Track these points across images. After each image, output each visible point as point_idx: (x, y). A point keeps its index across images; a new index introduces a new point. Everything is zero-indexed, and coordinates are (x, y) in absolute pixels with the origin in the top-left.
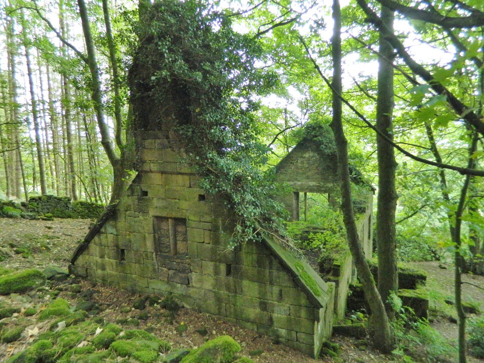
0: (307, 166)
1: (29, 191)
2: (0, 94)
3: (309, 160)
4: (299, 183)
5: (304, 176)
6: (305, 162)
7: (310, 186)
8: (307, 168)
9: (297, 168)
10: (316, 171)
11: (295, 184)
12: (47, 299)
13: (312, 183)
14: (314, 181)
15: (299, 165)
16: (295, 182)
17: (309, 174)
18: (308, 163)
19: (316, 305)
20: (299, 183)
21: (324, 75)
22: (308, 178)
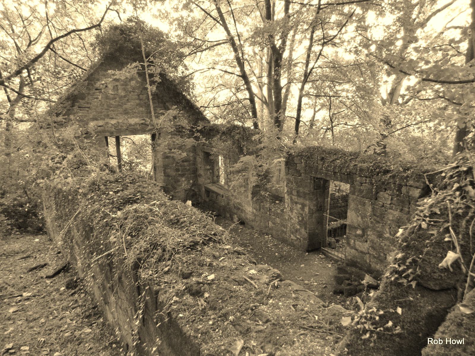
0: (123, 94)
1: (420, 190)
2: (1, 158)
3: (126, 85)
4: (113, 122)
5: (120, 110)
6: (119, 87)
7: (130, 125)
8: (125, 96)
9: (107, 97)
10: (138, 101)
11: (107, 123)
12: (160, 342)
13: (133, 121)
14: (137, 117)
15: (111, 92)
16: (107, 120)
17: (128, 105)
18: (124, 89)
19: (431, 178)
20: (113, 122)
21: (222, 45)
22: (126, 112)
